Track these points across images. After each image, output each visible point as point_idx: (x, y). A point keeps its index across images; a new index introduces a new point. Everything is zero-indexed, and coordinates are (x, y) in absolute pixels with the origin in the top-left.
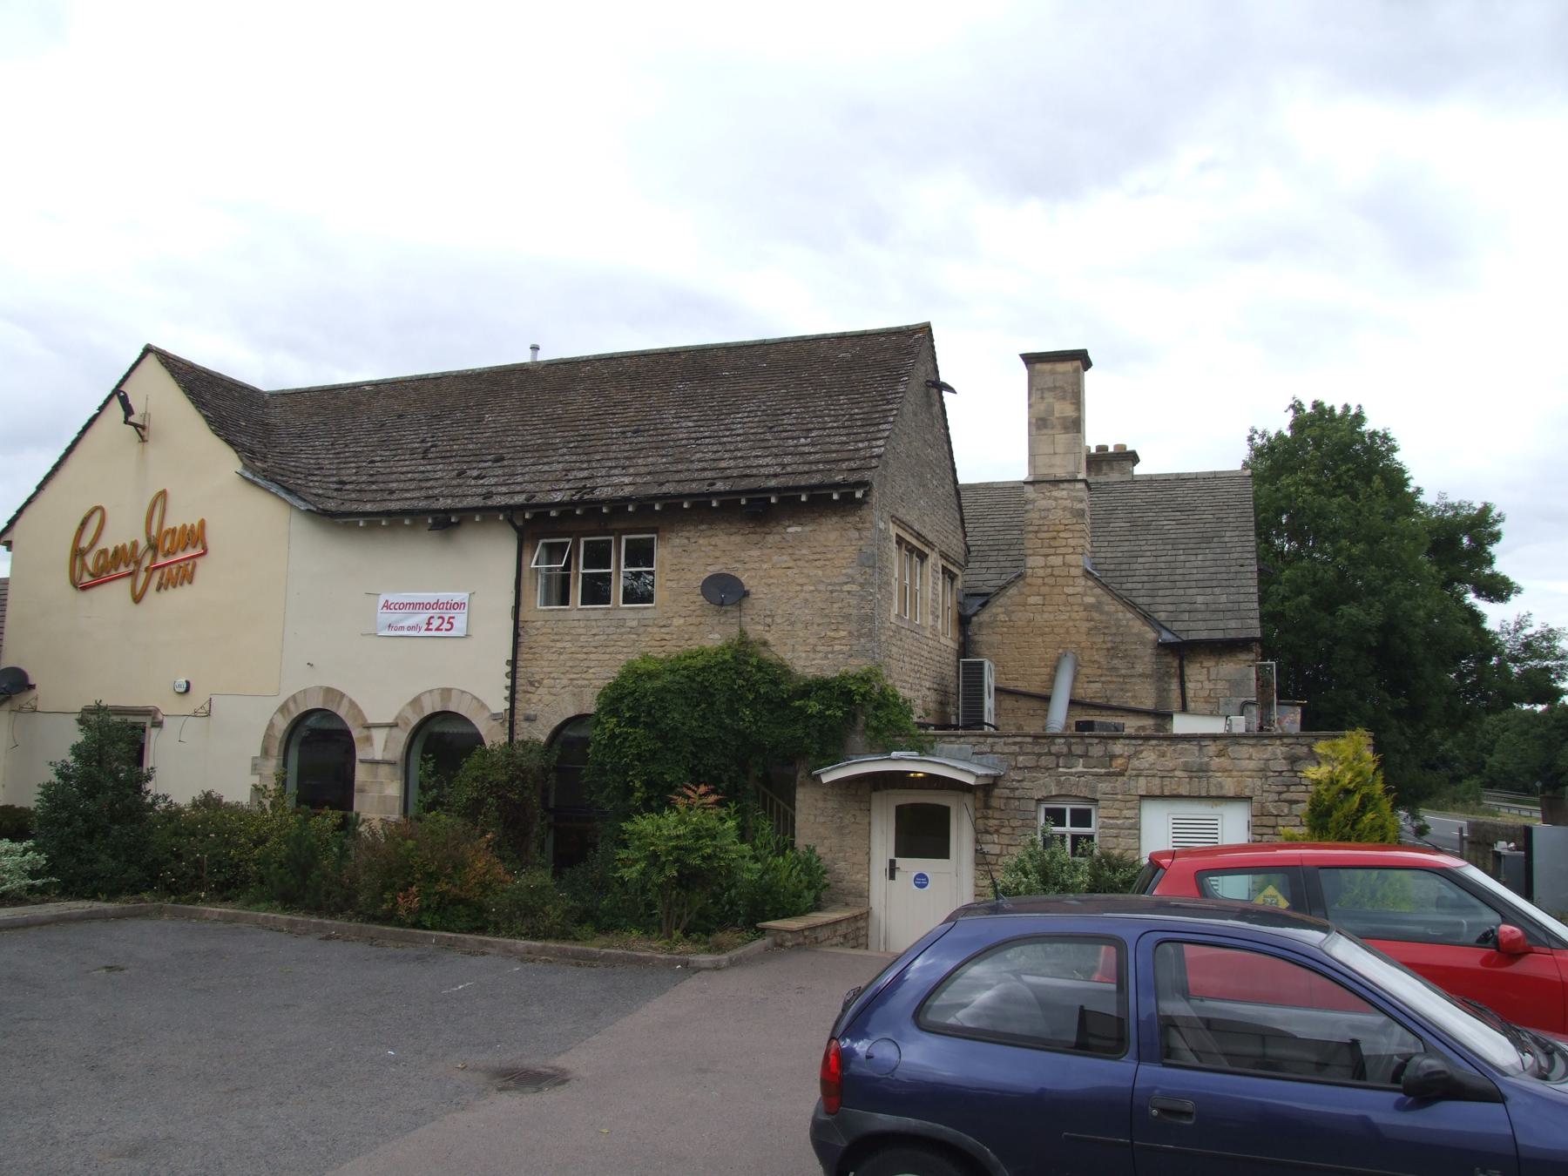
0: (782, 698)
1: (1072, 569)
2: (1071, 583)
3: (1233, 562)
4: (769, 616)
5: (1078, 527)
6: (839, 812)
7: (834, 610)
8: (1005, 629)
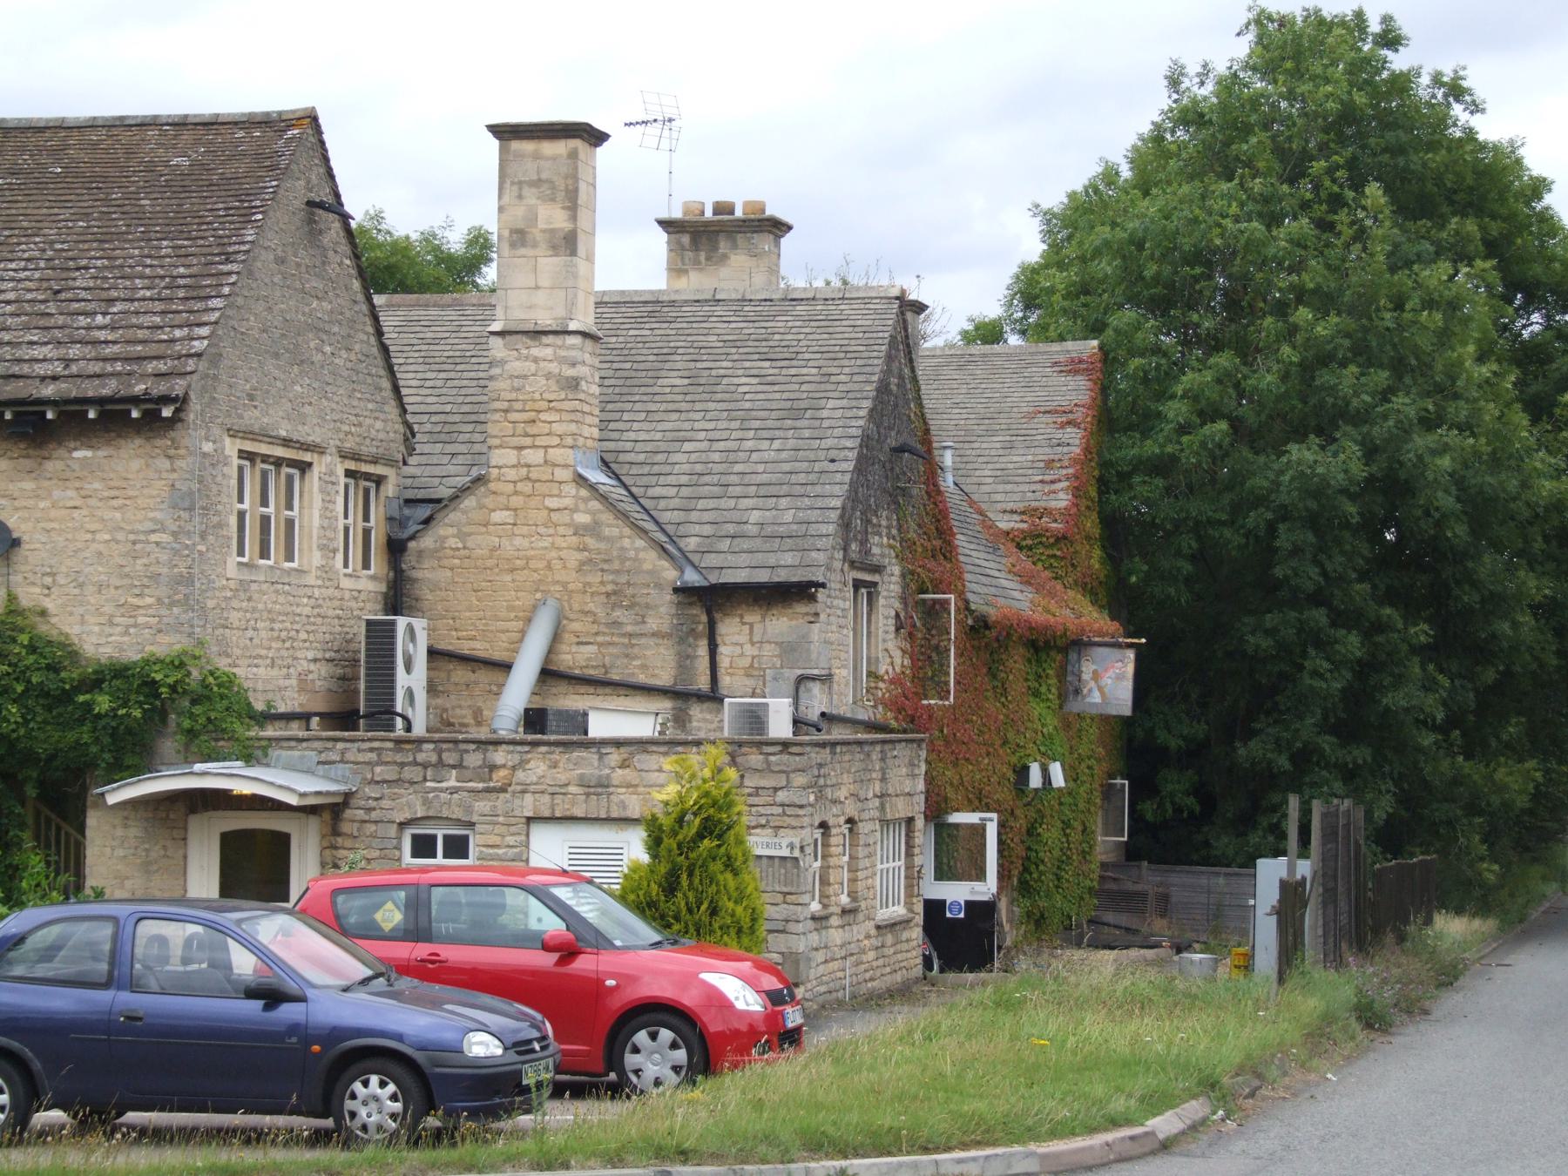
0: (64, 690)
1: (558, 471)
2: (556, 492)
3: (822, 455)
4: (48, 574)
5: (567, 405)
6: (144, 842)
7: (138, 568)
8: (457, 561)
